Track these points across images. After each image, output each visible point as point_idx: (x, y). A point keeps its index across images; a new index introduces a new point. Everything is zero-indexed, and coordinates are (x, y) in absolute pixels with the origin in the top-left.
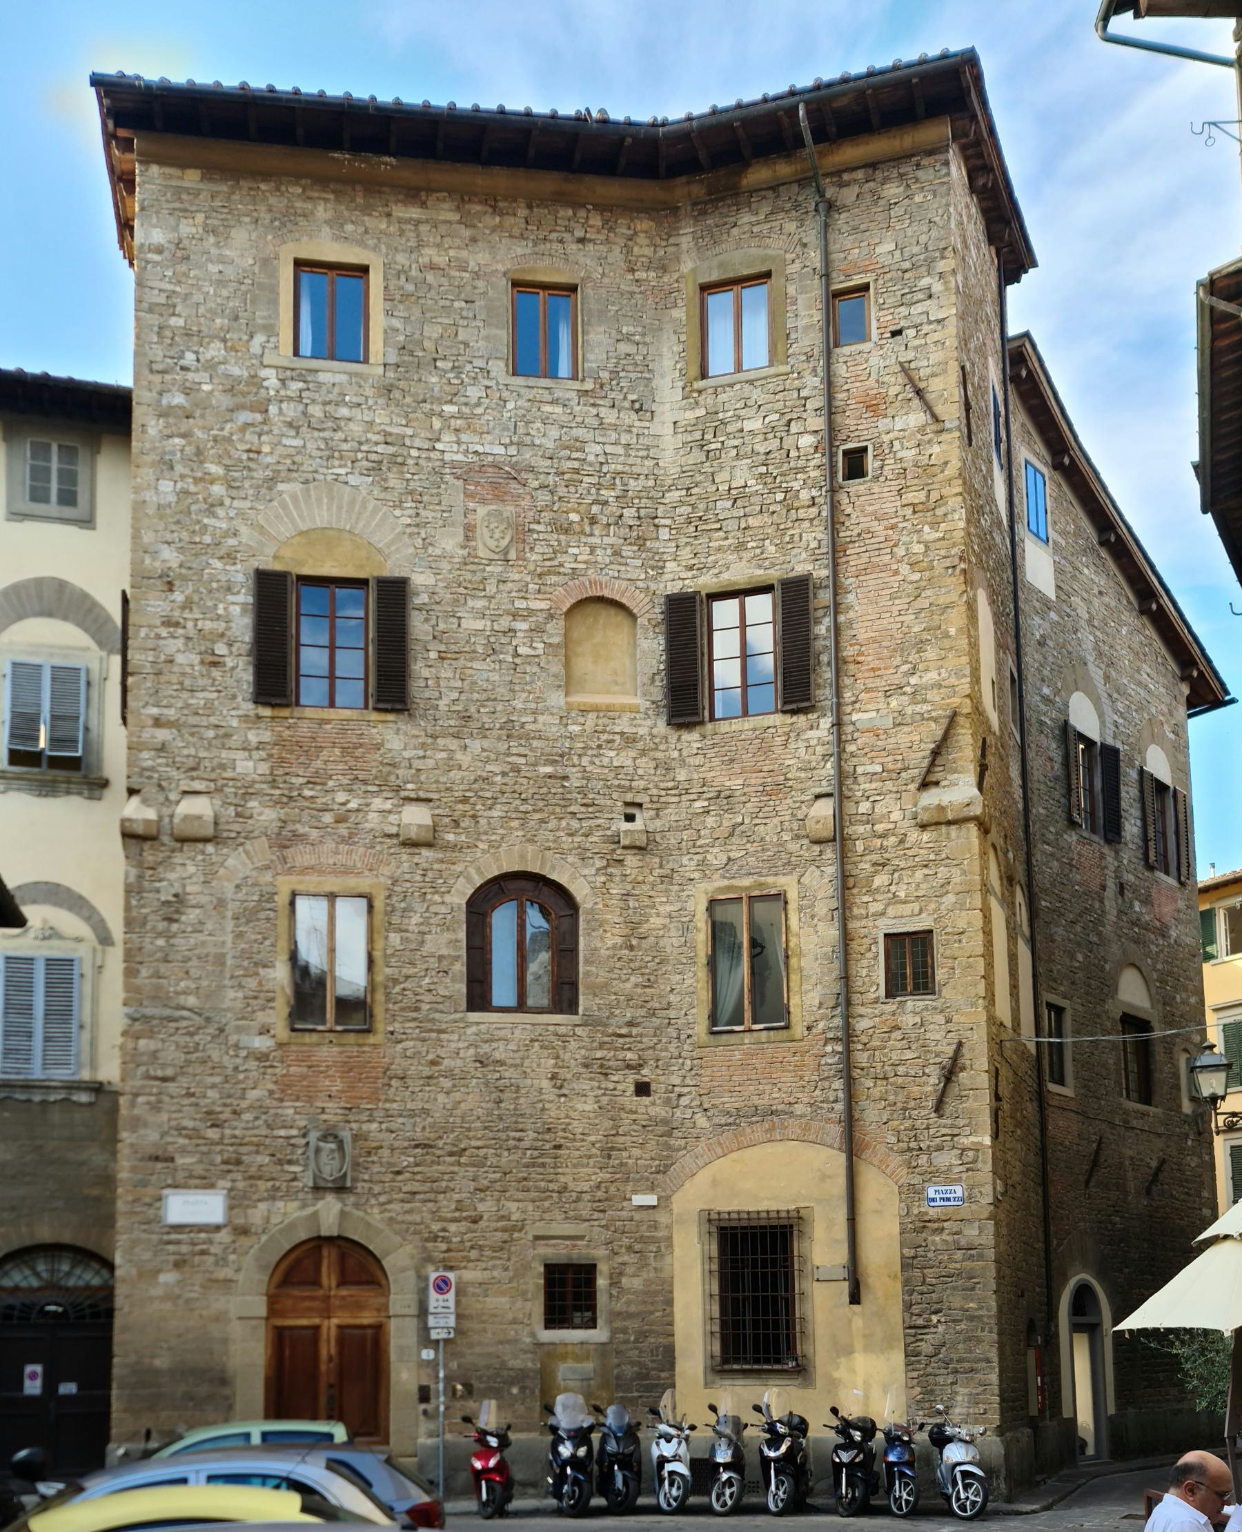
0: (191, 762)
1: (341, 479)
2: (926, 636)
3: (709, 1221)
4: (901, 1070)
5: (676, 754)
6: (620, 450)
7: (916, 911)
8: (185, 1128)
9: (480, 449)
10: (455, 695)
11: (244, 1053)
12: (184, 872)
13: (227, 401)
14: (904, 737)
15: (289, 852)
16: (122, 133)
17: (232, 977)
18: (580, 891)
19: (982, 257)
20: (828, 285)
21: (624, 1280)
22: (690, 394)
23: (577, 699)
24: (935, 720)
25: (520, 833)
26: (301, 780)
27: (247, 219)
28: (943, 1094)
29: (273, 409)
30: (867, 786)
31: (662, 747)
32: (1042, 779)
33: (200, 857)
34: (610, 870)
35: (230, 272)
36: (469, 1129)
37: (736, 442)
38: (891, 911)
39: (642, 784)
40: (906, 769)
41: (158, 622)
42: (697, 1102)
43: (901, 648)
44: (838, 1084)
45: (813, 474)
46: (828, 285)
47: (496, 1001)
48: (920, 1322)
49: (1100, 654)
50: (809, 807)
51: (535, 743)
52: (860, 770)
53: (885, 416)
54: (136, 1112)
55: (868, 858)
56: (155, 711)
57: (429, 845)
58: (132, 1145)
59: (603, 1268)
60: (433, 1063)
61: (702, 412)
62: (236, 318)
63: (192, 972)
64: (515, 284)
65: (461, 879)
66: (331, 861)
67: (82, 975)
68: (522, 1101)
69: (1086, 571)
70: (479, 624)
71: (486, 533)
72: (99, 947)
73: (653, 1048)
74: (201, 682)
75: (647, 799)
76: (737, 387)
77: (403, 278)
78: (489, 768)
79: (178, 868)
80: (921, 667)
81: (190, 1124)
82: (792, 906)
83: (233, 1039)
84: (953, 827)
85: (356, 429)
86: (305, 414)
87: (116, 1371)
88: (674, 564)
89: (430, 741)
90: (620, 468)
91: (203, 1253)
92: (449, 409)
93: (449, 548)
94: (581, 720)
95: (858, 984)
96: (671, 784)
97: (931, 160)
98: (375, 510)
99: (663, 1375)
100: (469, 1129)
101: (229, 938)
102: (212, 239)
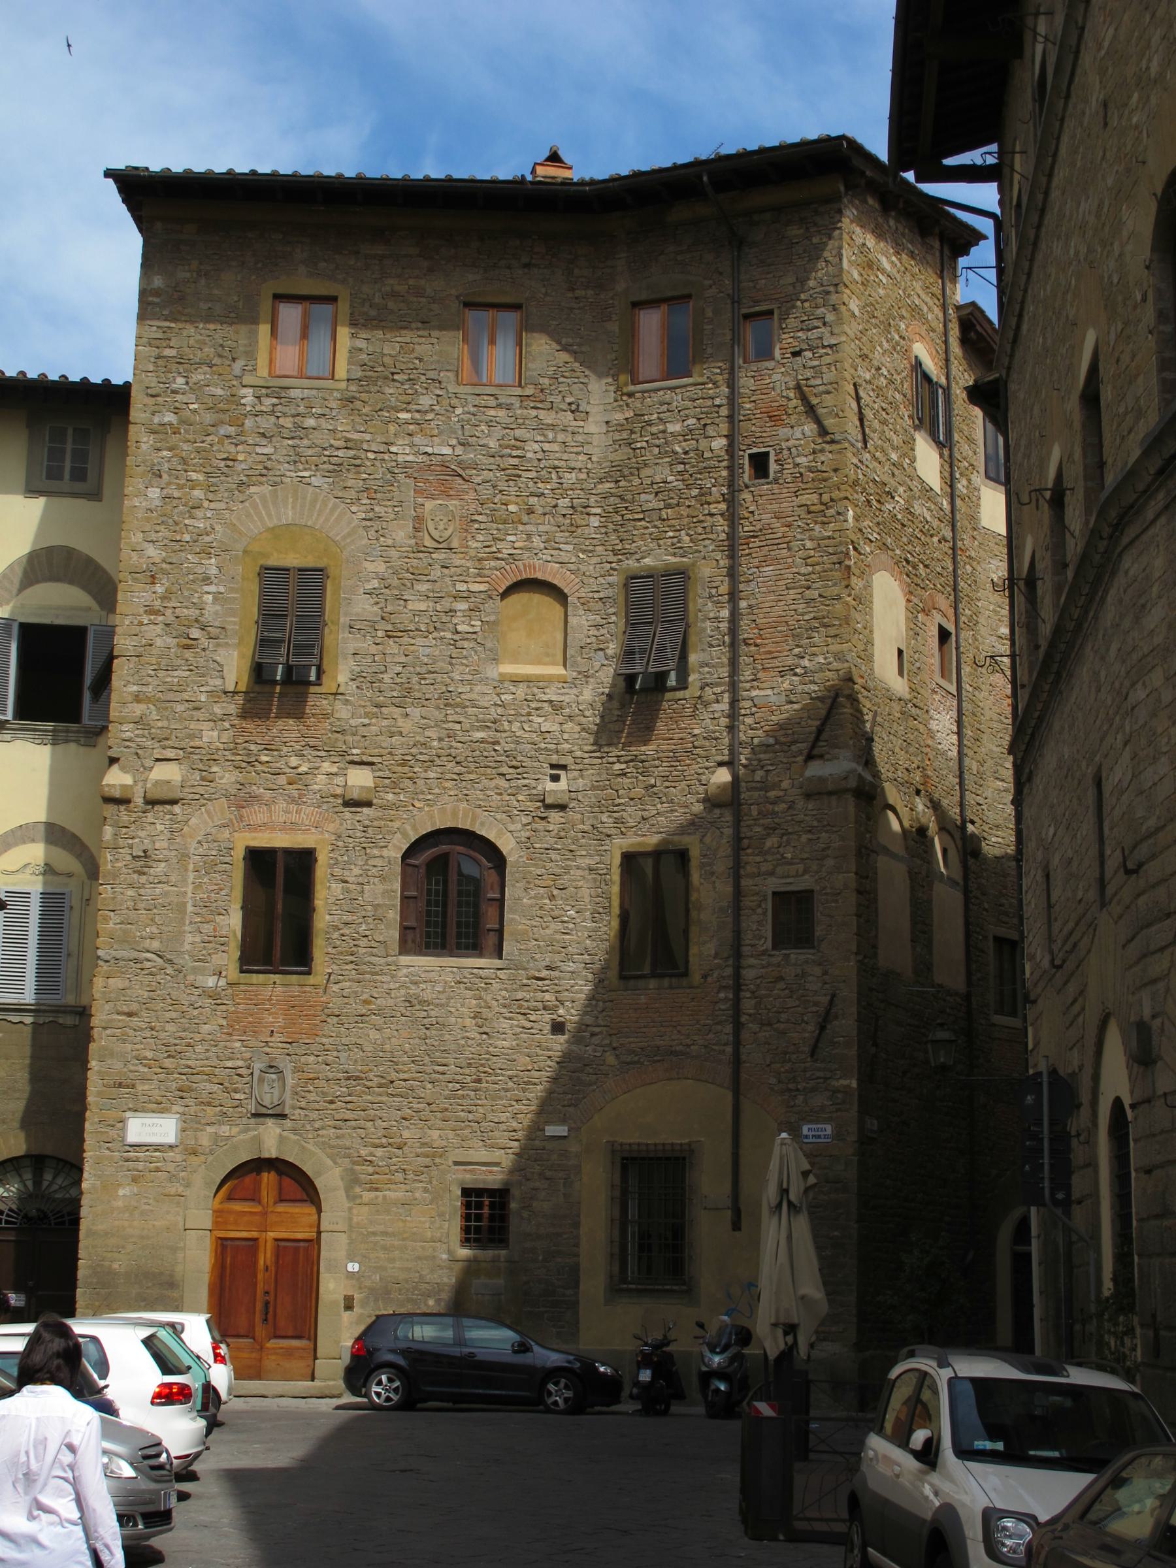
0: (166, 733)
3: (613, 1152)
4: (784, 1016)
6: (555, 447)
8: (146, 1058)
9: (429, 450)
17: (191, 923)
18: (506, 845)
21: (535, 1204)
27: (234, 263)
28: (817, 1041)
29: (249, 423)
30: (762, 756)
32: (996, 717)
33: (168, 817)
34: (534, 826)
38: (779, 870)
39: (567, 746)
40: (796, 742)
41: (142, 610)
44: (729, 1028)
55: (761, 821)
56: (135, 688)
58: (99, 1072)
60: (366, 1002)
63: (157, 918)
65: (398, 835)
66: (282, 820)
67: (72, 908)
70: (422, 606)
72: (86, 881)
77: (367, 305)
78: (427, 733)
81: (149, 1054)
82: (694, 863)
83: (191, 978)
84: (834, 798)
85: (320, 438)
87: (80, 1274)
91: (158, 1170)
92: (404, 416)
95: (747, 938)
98: (335, 507)
101: (190, 889)
102: (203, 281)
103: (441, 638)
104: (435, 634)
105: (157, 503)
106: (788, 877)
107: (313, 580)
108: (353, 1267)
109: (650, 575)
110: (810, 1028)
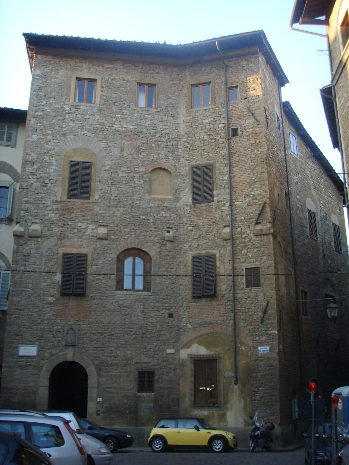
0: (35, 214)
1: (86, 134)
2: (256, 180)
4: (250, 310)
5: (183, 213)
7: (255, 261)
8: (26, 325)
9: (126, 126)
10: (116, 195)
11: (45, 302)
12: (30, 246)
13: (53, 114)
14: (251, 209)
15: (63, 241)
16: (31, 47)
17: (43, 279)
18: (152, 253)
19: (270, 80)
20: (226, 85)
21: (164, 376)
22: (188, 113)
23: (153, 196)
24: (260, 205)
25: (134, 236)
26: (69, 220)
27: (64, 68)
29: (67, 116)
30: (240, 223)
31: (179, 211)
33: (36, 242)
34: (162, 248)
35: (58, 81)
36: (115, 328)
37: (201, 126)
41: (29, 174)
42: (187, 320)
43: (249, 184)
44: (232, 314)
45: (223, 135)
46: (226, 85)
47: (125, 287)
48: (256, 390)
49: (315, 188)
50: (223, 229)
51: (140, 209)
52: (237, 219)
53: (243, 120)
54: (11, 320)
55: (241, 245)
56: (26, 199)
57: (106, 239)
59: (157, 372)
60: (104, 306)
61: (191, 117)
62: (59, 92)
64: (138, 84)
66: (75, 244)
68: (132, 319)
69: (310, 163)
70: (124, 175)
71: (127, 149)
73: (174, 303)
74: (40, 191)
75: (174, 226)
76: (201, 111)
77: (106, 82)
78: (125, 216)
79: (29, 245)
80: (255, 189)
81: (27, 324)
84: (265, 236)
86: (76, 117)
88: (183, 159)
89: (108, 208)
90: (167, 132)
93: (116, 153)
94: (154, 203)
96: (181, 222)
97: (254, 56)
99: (176, 407)
100: (115, 328)
102: (53, 73)
103: (130, 185)
104: (128, 184)
105: (36, 140)
106: (250, 263)
107: (87, 166)
108: (100, 400)
109: (199, 167)
110: (260, 314)
